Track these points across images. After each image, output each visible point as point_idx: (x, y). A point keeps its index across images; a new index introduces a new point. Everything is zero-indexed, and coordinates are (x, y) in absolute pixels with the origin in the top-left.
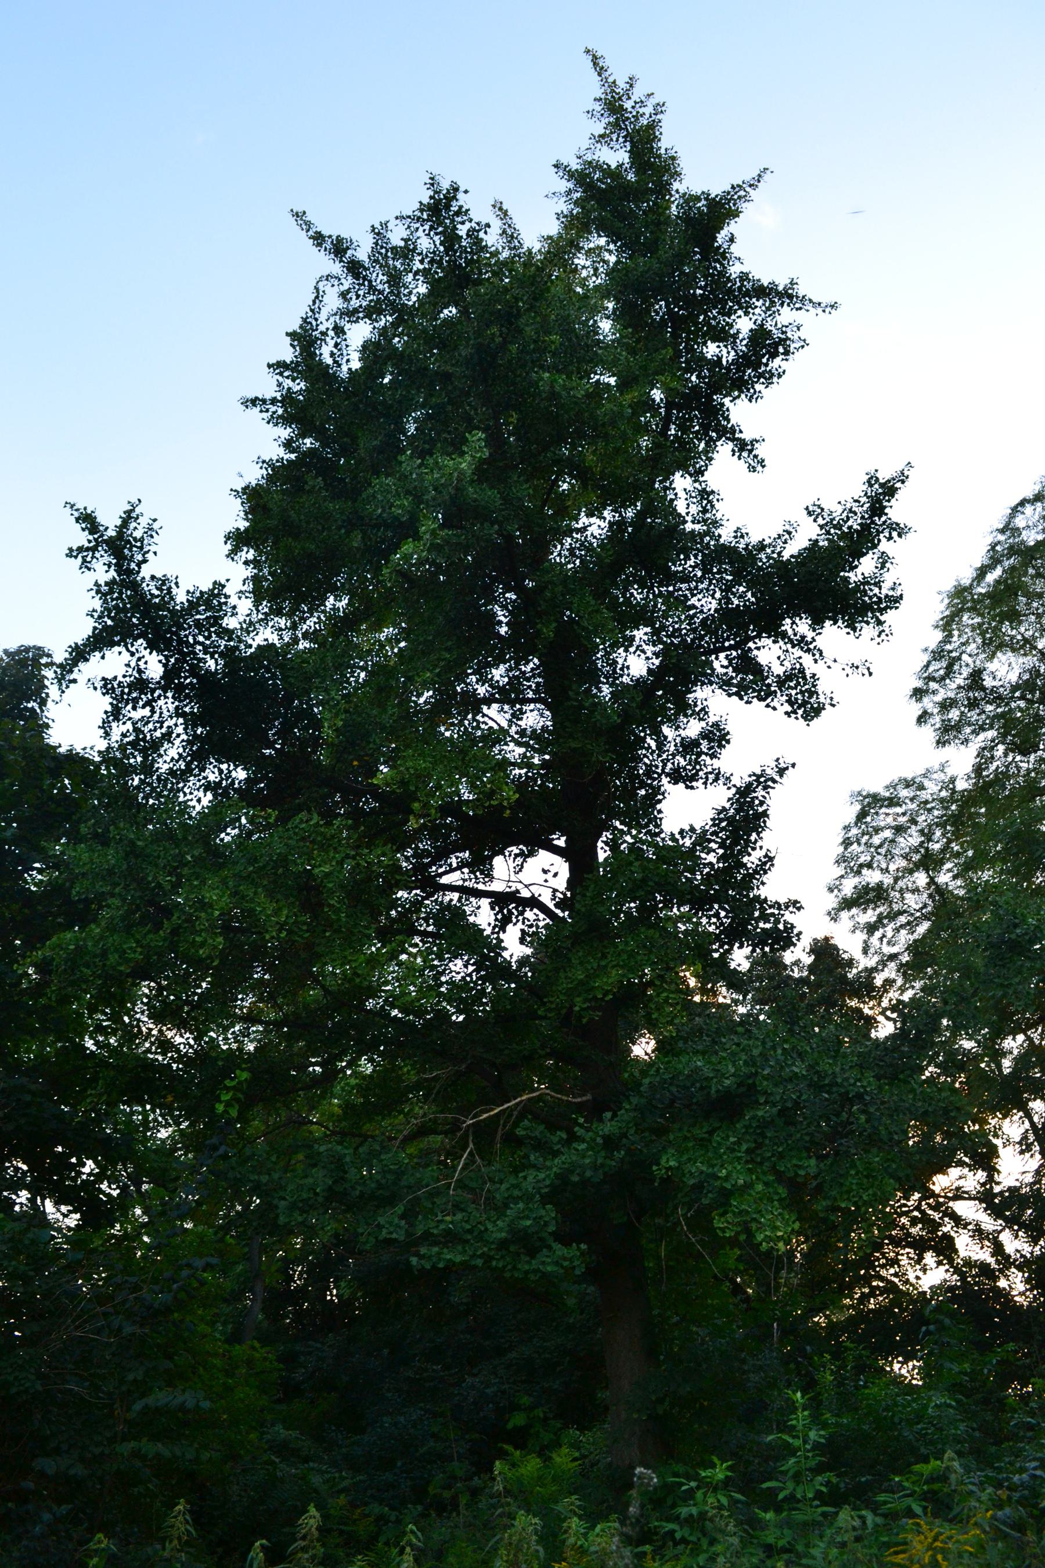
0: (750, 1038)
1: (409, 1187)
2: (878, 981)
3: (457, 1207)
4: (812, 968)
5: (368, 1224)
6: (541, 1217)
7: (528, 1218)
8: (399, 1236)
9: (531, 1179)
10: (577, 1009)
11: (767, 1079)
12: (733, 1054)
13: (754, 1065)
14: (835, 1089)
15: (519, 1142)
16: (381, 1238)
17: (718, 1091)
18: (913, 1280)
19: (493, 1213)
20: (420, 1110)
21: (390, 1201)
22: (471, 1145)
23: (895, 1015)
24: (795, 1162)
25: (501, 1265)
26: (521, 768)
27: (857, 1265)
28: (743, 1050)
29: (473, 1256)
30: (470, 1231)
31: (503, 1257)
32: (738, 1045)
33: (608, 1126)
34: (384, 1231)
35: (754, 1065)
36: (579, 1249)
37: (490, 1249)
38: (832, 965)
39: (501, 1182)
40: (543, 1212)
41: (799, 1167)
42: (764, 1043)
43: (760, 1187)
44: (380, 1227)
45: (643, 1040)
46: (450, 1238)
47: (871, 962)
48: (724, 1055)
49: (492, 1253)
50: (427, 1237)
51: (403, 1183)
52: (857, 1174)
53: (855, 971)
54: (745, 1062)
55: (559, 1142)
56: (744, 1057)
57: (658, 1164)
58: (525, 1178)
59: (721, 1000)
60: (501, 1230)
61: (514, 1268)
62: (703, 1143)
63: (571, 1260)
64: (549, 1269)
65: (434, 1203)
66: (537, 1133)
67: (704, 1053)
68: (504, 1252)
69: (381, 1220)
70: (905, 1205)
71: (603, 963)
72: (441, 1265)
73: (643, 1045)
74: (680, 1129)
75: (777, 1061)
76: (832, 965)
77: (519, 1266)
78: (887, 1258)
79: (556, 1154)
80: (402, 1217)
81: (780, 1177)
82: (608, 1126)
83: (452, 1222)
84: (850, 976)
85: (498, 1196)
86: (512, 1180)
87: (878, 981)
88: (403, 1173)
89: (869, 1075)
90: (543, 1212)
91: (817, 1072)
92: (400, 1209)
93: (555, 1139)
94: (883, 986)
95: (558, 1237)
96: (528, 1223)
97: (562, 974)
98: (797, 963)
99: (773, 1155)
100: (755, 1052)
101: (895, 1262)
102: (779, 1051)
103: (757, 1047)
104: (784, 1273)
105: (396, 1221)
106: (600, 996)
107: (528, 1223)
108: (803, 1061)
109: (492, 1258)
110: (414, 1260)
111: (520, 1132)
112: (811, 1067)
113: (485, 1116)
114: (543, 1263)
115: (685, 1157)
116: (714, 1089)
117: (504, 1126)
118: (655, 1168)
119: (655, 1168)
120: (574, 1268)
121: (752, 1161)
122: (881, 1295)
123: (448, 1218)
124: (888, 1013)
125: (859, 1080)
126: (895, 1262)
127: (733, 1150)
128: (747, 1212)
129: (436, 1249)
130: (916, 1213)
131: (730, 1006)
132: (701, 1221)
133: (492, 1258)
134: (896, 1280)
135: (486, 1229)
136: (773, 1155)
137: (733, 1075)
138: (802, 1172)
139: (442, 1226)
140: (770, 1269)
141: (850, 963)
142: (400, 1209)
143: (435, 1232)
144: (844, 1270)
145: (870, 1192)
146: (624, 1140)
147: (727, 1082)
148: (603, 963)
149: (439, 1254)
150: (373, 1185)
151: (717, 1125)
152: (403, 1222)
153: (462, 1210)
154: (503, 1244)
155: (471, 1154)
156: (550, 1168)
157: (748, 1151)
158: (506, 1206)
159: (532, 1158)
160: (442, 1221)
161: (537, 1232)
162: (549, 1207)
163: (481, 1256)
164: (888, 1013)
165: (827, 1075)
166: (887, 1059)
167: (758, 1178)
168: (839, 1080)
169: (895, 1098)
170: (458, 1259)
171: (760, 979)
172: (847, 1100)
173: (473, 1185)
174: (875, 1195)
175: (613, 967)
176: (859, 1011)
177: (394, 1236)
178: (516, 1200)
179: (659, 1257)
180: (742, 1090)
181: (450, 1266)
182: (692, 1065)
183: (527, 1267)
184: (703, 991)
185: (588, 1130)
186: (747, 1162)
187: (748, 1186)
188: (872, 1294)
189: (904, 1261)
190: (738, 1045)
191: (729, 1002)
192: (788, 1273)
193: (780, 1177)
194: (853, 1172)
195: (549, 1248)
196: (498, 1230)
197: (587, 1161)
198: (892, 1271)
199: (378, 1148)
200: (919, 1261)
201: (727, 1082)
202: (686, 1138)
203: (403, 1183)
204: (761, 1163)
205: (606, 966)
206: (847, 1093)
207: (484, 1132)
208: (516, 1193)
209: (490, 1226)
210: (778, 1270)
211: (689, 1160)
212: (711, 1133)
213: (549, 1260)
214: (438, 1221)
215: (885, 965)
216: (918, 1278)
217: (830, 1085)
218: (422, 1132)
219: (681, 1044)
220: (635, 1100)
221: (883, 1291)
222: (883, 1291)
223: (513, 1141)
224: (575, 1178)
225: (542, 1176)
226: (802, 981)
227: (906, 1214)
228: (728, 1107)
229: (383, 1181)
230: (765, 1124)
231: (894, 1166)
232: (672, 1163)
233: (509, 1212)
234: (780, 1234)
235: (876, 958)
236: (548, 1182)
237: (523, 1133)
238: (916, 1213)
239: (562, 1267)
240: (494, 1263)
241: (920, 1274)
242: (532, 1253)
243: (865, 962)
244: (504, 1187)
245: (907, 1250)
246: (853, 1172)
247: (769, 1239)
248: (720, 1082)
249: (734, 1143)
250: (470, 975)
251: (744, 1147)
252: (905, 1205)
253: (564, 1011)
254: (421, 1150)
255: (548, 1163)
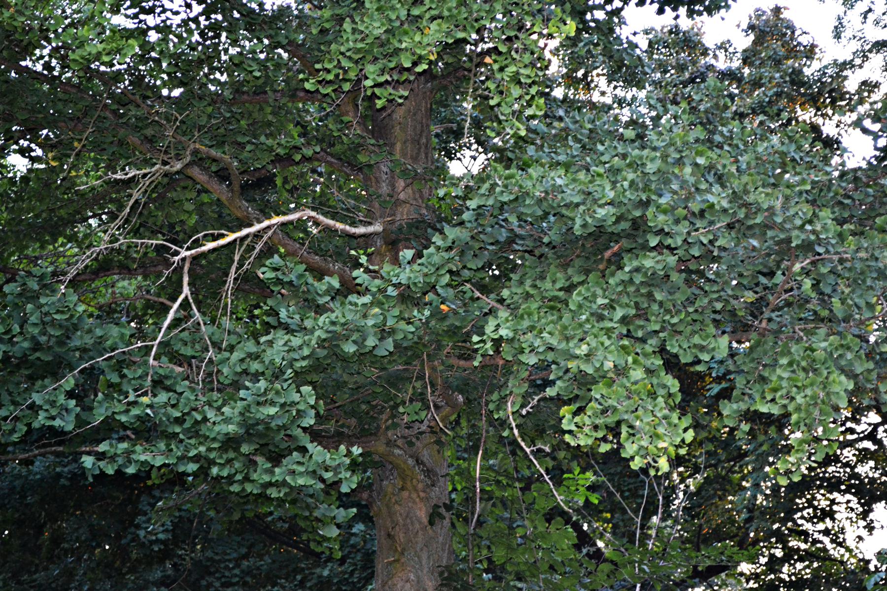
0: (643, 148)
1: (84, 350)
2: (851, 85)
3: (159, 383)
4: (748, 58)
5: (15, 403)
6: (294, 404)
7: (272, 403)
8: (67, 424)
9: (277, 347)
10: (368, 83)
11: (665, 212)
12: (615, 171)
13: (647, 188)
14: (770, 233)
15: (264, 289)
16: (36, 425)
17: (584, 226)
18: (851, 543)
19: (215, 395)
20: (101, 233)
21: (55, 369)
22: (186, 290)
23: (876, 127)
24: (697, 340)
25: (225, 473)
26: (97, 71)
27: (770, 514)
28: (629, 165)
29: (182, 459)
30: (179, 421)
31: (229, 461)
32: (624, 156)
33: (407, 272)
34: (42, 415)
35: (647, 188)
36: (349, 453)
37: (209, 450)
38: (782, 52)
39: (231, 349)
40: (296, 397)
41: (702, 348)
42: (664, 157)
43: (638, 374)
44: (34, 408)
45: (468, 153)
46: (146, 431)
47: (844, 51)
48: (601, 170)
49: (212, 455)
50: (109, 428)
51: (76, 342)
52: (790, 364)
53: (816, 65)
54: (632, 183)
55: (327, 292)
56: (631, 176)
57: (481, 333)
58: (270, 343)
59: (596, 97)
60: (228, 421)
61: (247, 479)
62: (555, 305)
63: (336, 470)
64: (301, 481)
65: (123, 376)
66: (292, 277)
67: (567, 166)
68: (231, 455)
69: (37, 398)
70: (852, 431)
71: (416, 12)
72: (131, 470)
73: (467, 161)
74: (521, 283)
75: (684, 184)
76: (782, 52)
77: (255, 476)
78: (815, 508)
79: (320, 310)
80: (70, 395)
81: (672, 364)
82: (407, 272)
83: (150, 406)
84: (807, 71)
85: (225, 371)
86: (251, 346)
87: (851, 85)
88: (76, 328)
89: (826, 214)
90: (296, 397)
91: (747, 205)
92: (69, 382)
93: (321, 287)
94: (859, 92)
95: (315, 435)
96: (272, 411)
97: (347, 26)
98: (723, 46)
99: (663, 329)
100: (651, 168)
101: (829, 514)
102: (688, 170)
103: (653, 160)
104: (655, 519)
105: (61, 399)
106: (407, 64)
107: (272, 411)
108: (723, 186)
109: (213, 463)
110: (88, 461)
111: (265, 274)
112: (735, 197)
113: (210, 245)
114: (293, 472)
115: (526, 323)
116: (578, 222)
117: (241, 265)
118: (475, 339)
119: (475, 339)
120: (340, 481)
121: (629, 335)
122: (801, 559)
123: (145, 400)
124: (867, 123)
125: (810, 222)
126: (829, 514)
127: (601, 318)
128: (615, 409)
129: (124, 445)
130: (868, 444)
131: (610, 108)
132: (542, 424)
133: (213, 463)
134: (826, 540)
135: (205, 419)
136: (663, 329)
137: (611, 203)
138: (705, 357)
139: (135, 411)
140: (636, 512)
141: (810, 52)
142: (69, 382)
143: (123, 418)
144: (748, 520)
145: (809, 392)
146: (429, 297)
147: (601, 212)
148: (416, 12)
149: (128, 453)
150: (26, 345)
151: (576, 279)
152: (73, 402)
153: (168, 389)
154: (230, 443)
155: (185, 305)
156: (312, 331)
157: (624, 320)
158: (237, 385)
159: (283, 314)
160: (135, 403)
161: (284, 427)
162: (306, 389)
163: (197, 458)
164: (867, 123)
165: (759, 210)
166: (857, 195)
167: (635, 362)
168: (779, 220)
169: (862, 254)
170: (159, 461)
171: (663, 67)
172: (785, 250)
173: (188, 351)
174: (814, 397)
175: (433, 19)
176: (815, 129)
177: (57, 423)
178: (256, 377)
179: (470, 479)
180: (625, 225)
181: (147, 470)
182: (547, 184)
183: (266, 478)
184: (570, 80)
185: (374, 274)
186: (621, 337)
187: (621, 371)
188: (790, 555)
189: (842, 514)
190: (624, 156)
191: (608, 100)
192: (663, 519)
193: (672, 364)
194: (784, 361)
195: (303, 450)
196: (225, 421)
197: (370, 322)
198: (821, 526)
199: (36, 287)
200: (864, 515)
201: (601, 212)
202: (528, 296)
203: (76, 342)
204: (643, 340)
205: (420, 17)
206: (789, 240)
207: (208, 274)
208: (255, 366)
209: (211, 414)
210: (649, 513)
211: (531, 329)
212: (569, 289)
213: (302, 469)
214: (129, 404)
215: (865, 58)
216: (860, 538)
217: (767, 226)
218: (104, 267)
219: (531, 150)
220: (452, 233)
221: (808, 556)
222: (808, 556)
223: (250, 284)
224: (350, 348)
225: (296, 341)
226: (731, 75)
227: (851, 444)
228: (598, 249)
229: (43, 339)
230: (655, 280)
231: (849, 356)
232: (504, 332)
233: (242, 393)
234: (662, 445)
235: (855, 45)
236: (306, 352)
237: (270, 275)
238: (868, 444)
239: (323, 481)
240: (215, 471)
241: (864, 533)
242: (276, 459)
243: (832, 52)
244: (236, 356)
245: (848, 497)
246: (784, 361)
247: (643, 452)
248: (590, 212)
249: (604, 307)
250: (195, 20)
251: (619, 313)
252: (852, 431)
253: (347, 87)
254: (100, 308)
255: (308, 323)
